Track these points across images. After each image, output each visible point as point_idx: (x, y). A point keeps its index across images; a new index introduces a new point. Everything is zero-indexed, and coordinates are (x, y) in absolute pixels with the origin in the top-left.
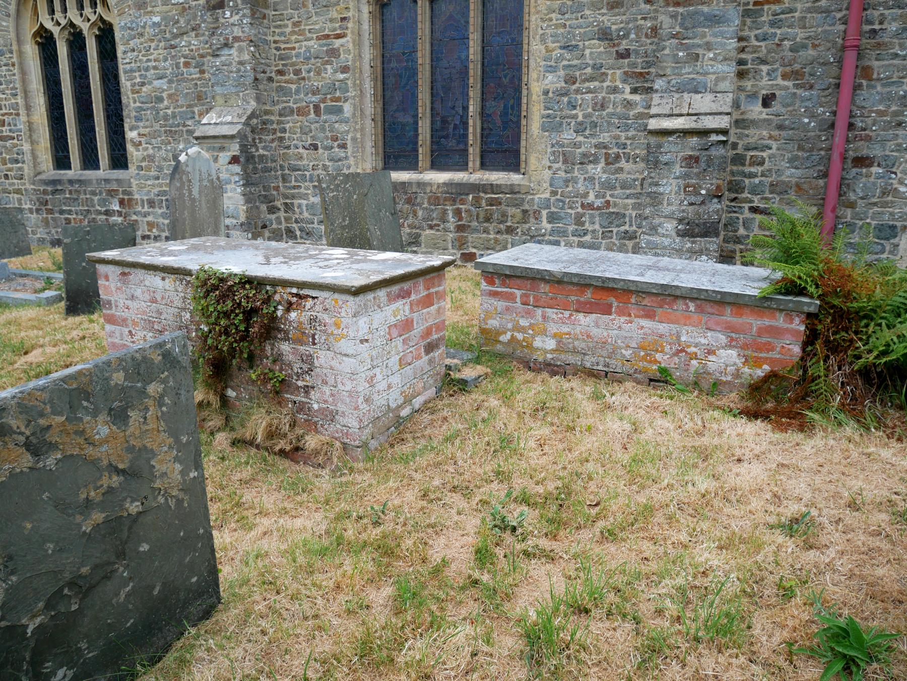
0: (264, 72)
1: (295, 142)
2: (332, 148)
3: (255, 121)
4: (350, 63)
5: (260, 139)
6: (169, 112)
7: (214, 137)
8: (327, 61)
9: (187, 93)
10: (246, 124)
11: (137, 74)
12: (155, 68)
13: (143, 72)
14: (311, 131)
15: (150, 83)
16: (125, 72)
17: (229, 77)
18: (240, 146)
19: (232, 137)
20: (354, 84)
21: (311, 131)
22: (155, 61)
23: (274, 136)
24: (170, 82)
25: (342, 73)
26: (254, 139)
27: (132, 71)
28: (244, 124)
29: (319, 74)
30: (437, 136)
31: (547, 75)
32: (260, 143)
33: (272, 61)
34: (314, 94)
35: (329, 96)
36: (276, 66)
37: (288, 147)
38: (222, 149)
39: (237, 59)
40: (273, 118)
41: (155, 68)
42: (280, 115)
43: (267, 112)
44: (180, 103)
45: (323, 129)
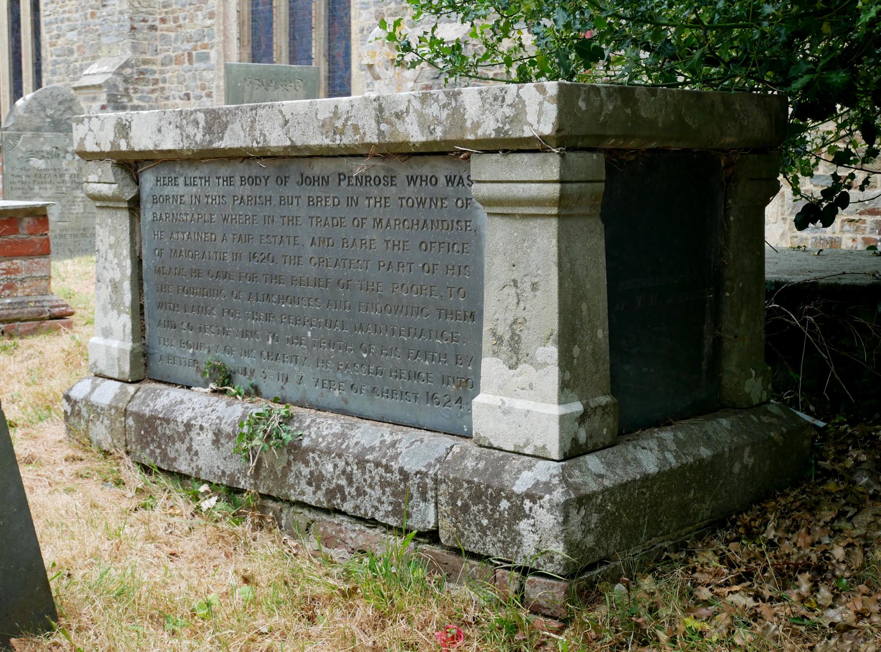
0: (144, 21)
1: (173, 92)
2: (201, 97)
3: (128, 71)
4: (215, 9)
5: (135, 89)
6: (78, 64)
7: (87, 87)
8: (198, 7)
9: (92, 45)
10: (118, 73)
11: (54, 26)
12: (69, 19)
13: (59, 24)
14: (185, 80)
15: (64, 35)
16: (46, 25)
17: (112, 27)
18: (108, 95)
19: (99, 87)
20: (218, 30)
21: (185, 80)
22: (69, 12)
23: (155, 87)
24: (80, 33)
25: (210, 18)
26: (126, 89)
27: (51, 23)
28: (114, 73)
29: (192, 20)
30: (331, 78)
31: (362, 11)
32: (135, 92)
33: (157, 9)
34: (188, 42)
35: (199, 43)
36: (160, 14)
37: (167, 98)
38: (94, 99)
39: (118, 9)
40: (154, 67)
41: (69, 19)
42: (163, 64)
43: (145, 62)
44: (86, 55)
45: (194, 78)
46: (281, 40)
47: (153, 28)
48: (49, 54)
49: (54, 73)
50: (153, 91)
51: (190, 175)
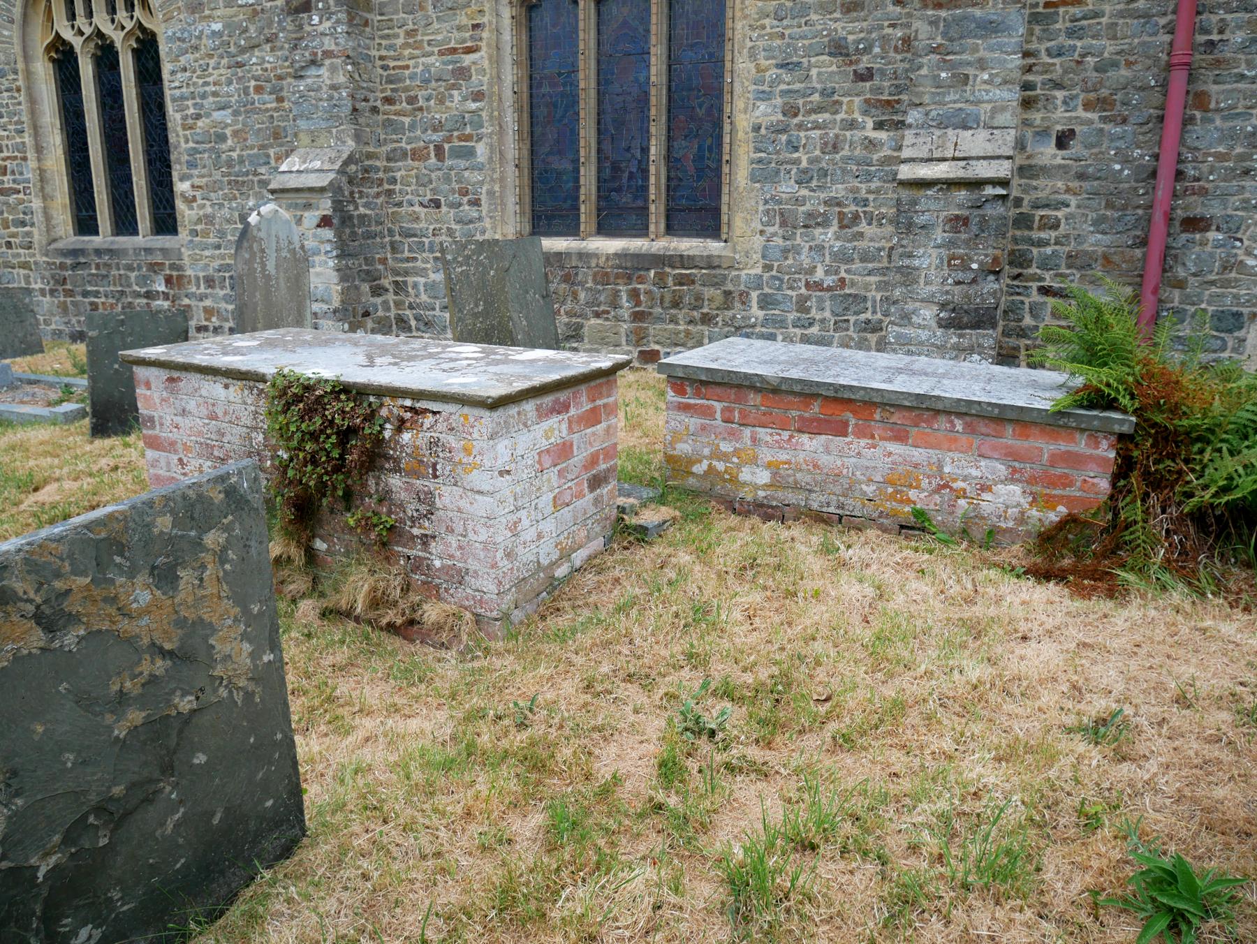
0: (366, 100)
1: (409, 197)
2: (460, 205)
3: (353, 168)
4: (484, 88)
5: (360, 192)
6: (235, 155)
7: (297, 190)
8: (453, 85)
9: (260, 129)
10: (341, 172)
11: (190, 103)
12: (215, 94)
13: (198, 100)
15: (208, 115)
16: (174, 100)
18: (333, 202)
19: (322, 190)
20: (491, 117)
21: (431, 182)
22: (215, 84)
24: (236, 113)
25: (474, 101)
26: (352, 193)
27: (182, 98)
28: (338, 172)
29: (442, 102)
31: (758, 103)
32: (360, 198)
33: (378, 85)
34: (435, 130)
35: (456, 134)
36: (382, 91)
37: (400, 204)
38: (308, 206)
39: (328, 82)
40: (378, 163)
41: (215, 94)
42: (389, 159)
43: (370, 156)
44: (249, 143)
45: (447, 179)
46: (87, 70)
47: (375, 110)
48: (182, 140)
49: (192, 165)
50: (378, 195)
51: (35, 231)
